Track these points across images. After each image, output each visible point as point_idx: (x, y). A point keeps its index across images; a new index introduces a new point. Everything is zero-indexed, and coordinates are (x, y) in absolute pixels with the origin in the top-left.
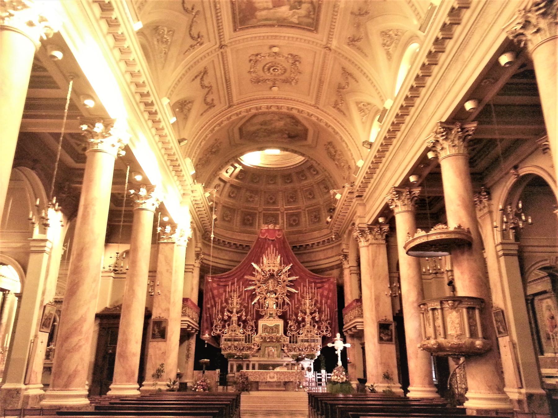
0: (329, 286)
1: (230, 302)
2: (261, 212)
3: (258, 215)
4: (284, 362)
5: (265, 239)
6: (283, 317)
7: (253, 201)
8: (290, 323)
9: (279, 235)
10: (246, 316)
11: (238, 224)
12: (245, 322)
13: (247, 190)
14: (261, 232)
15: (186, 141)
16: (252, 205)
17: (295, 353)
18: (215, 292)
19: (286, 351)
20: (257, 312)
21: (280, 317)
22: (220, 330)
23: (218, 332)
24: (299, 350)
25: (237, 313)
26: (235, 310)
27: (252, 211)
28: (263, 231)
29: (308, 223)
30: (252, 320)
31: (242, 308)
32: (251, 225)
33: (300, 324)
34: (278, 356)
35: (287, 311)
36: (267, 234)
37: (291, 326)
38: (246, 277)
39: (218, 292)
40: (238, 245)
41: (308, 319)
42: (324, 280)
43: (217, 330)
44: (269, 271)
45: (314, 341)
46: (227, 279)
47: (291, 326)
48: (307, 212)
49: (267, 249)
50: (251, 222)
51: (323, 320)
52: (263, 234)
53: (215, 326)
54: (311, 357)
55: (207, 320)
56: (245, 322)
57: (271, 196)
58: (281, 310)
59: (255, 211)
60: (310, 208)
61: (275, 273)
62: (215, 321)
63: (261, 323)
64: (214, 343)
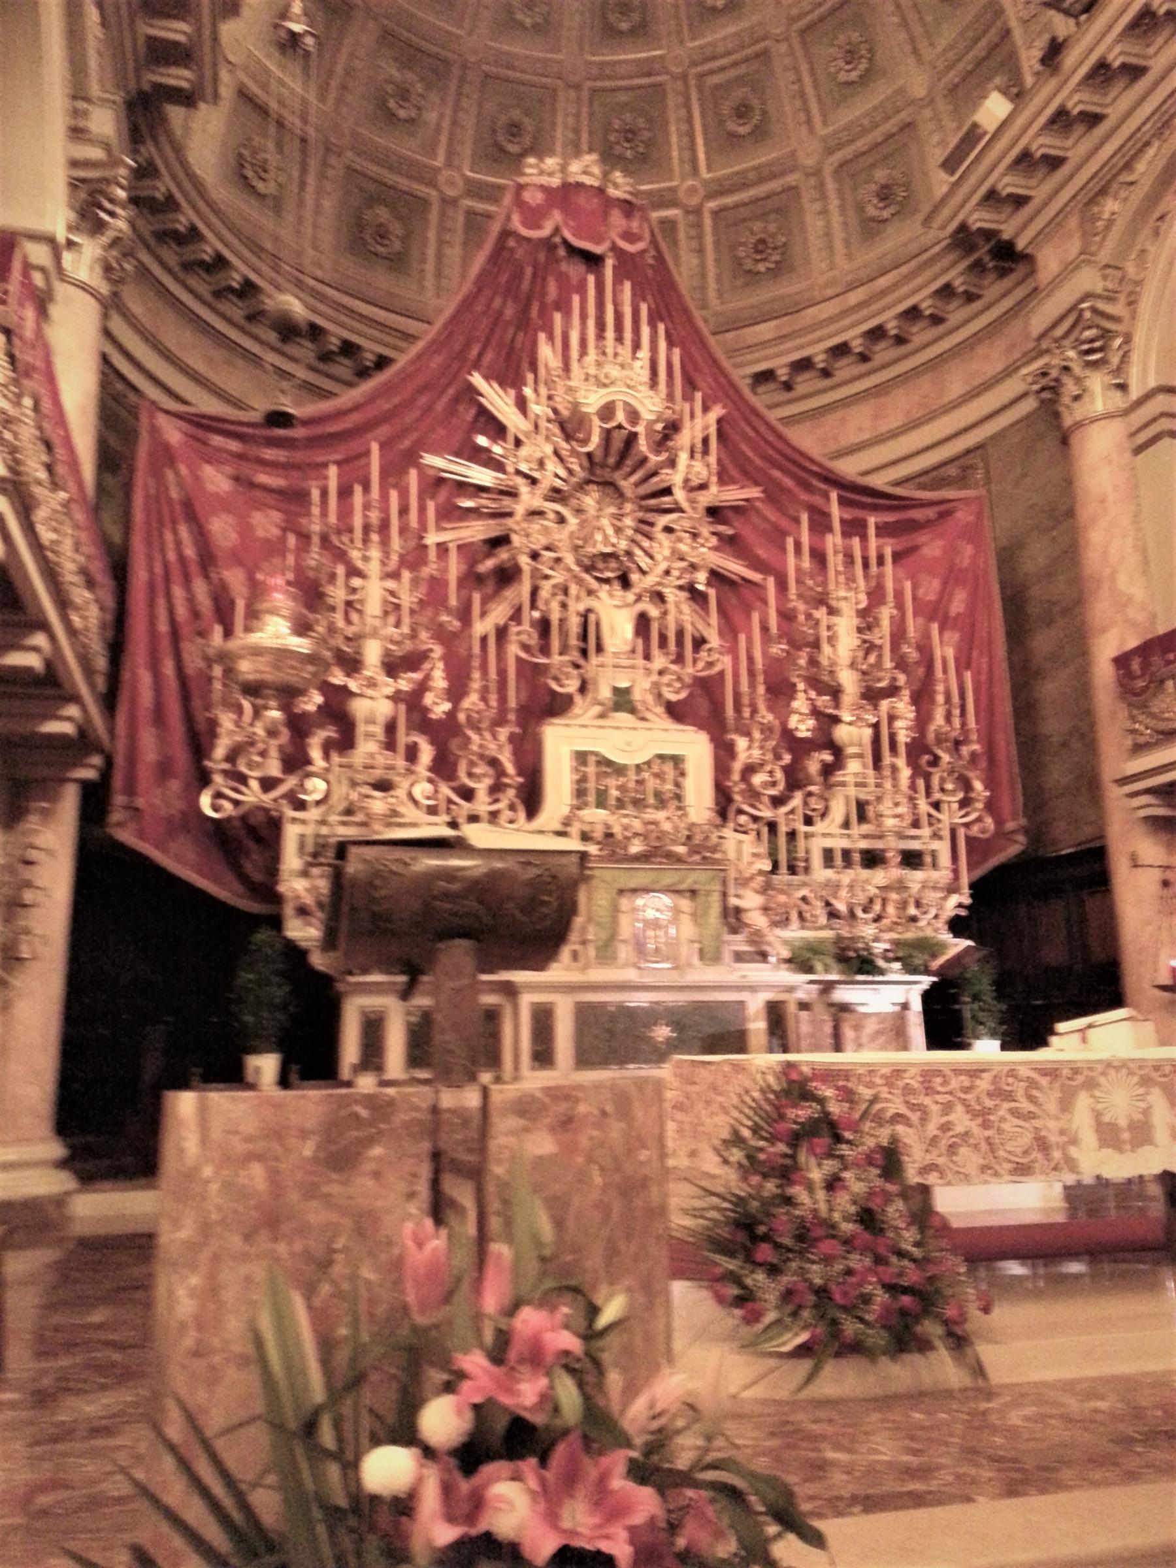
0: (952, 550)
1: (337, 594)
2: (454, 202)
3: (434, 216)
4: (753, 989)
5: (548, 245)
6: (702, 706)
7: (411, 121)
8: (745, 750)
9: (629, 237)
10: (456, 692)
11: (327, 239)
12: (444, 734)
13: (386, 37)
14: (519, 202)
15: (66, 1545)
16: (405, 147)
17: (809, 934)
18: (222, 529)
19: (757, 920)
20: (531, 673)
21: (676, 712)
22: (268, 784)
23: (253, 795)
24: (833, 914)
25: (392, 667)
26: (372, 653)
27: (403, 183)
28: (533, 197)
29: (712, 285)
30: (500, 721)
31: (425, 639)
32: (397, 263)
33: (809, 760)
34: (710, 956)
35: (721, 674)
36: (557, 216)
37: (750, 770)
38: (432, 460)
39: (245, 530)
40: (334, 343)
41: (852, 733)
42: (918, 514)
43: (243, 779)
44: (607, 412)
45: (912, 859)
46: (300, 456)
47: (750, 770)
48: (708, 222)
49: (563, 306)
50: (397, 246)
51: (940, 739)
52: (534, 217)
53: (231, 757)
54: (911, 956)
55: (159, 716)
56: (444, 734)
57: (516, 114)
58: (689, 670)
59: (420, 189)
60: (729, 200)
61: (640, 429)
62: (226, 721)
63: (560, 742)
64: (217, 881)
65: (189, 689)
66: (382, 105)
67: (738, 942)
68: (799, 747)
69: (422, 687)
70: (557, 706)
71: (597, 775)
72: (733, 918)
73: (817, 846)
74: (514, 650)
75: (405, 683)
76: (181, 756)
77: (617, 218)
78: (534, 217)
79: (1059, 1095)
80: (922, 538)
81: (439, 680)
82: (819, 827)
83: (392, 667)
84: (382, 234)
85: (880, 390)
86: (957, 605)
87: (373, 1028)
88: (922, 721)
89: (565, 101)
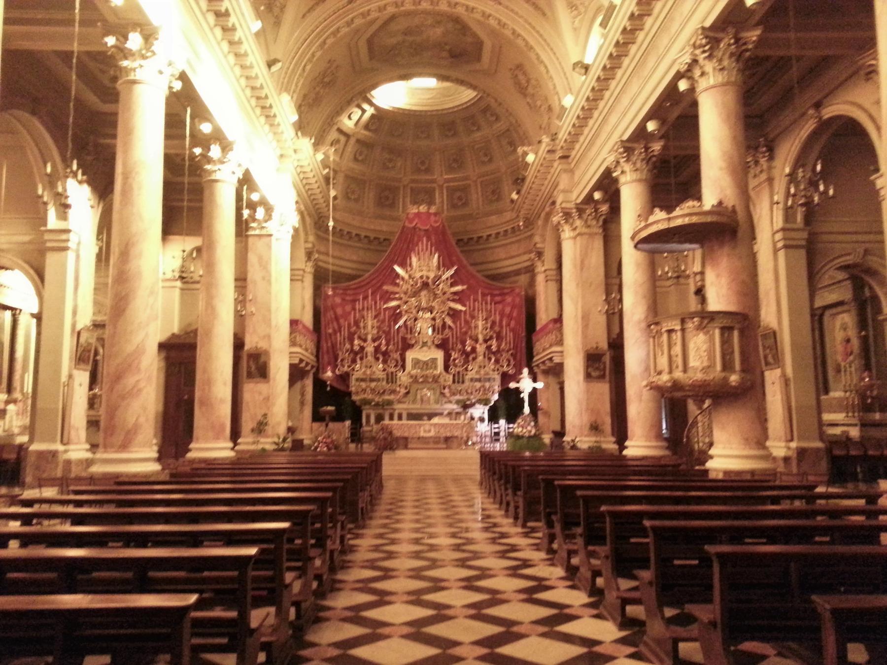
1: (362, 325)
8: (454, 355)
10: (387, 344)
12: (386, 354)
18: (339, 311)
19: (448, 395)
23: (346, 369)
25: (374, 341)
26: (369, 337)
33: (468, 356)
34: (437, 402)
37: (454, 360)
39: (344, 310)
42: (506, 291)
44: (421, 277)
47: (454, 360)
48: (479, 185)
51: (503, 350)
55: (328, 352)
56: (386, 354)
62: (340, 353)
63: (410, 355)
65: (334, 346)
66: (384, 164)
67: (445, 400)
68: (467, 355)
69: (380, 344)
70: (411, 346)
71: (416, 363)
72: (443, 394)
73: (467, 377)
74: (400, 335)
75: (376, 344)
76: (333, 360)
77: (433, 218)
78: (411, 221)
79: (565, 439)
80: (507, 297)
81: (384, 342)
82: (469, 373)
83: (374, 341)
84: (387, 198)
85: (519, 241)
86: (515, 314)
87: (368, 417)
88: (499, 346)
89: (437, 157)
